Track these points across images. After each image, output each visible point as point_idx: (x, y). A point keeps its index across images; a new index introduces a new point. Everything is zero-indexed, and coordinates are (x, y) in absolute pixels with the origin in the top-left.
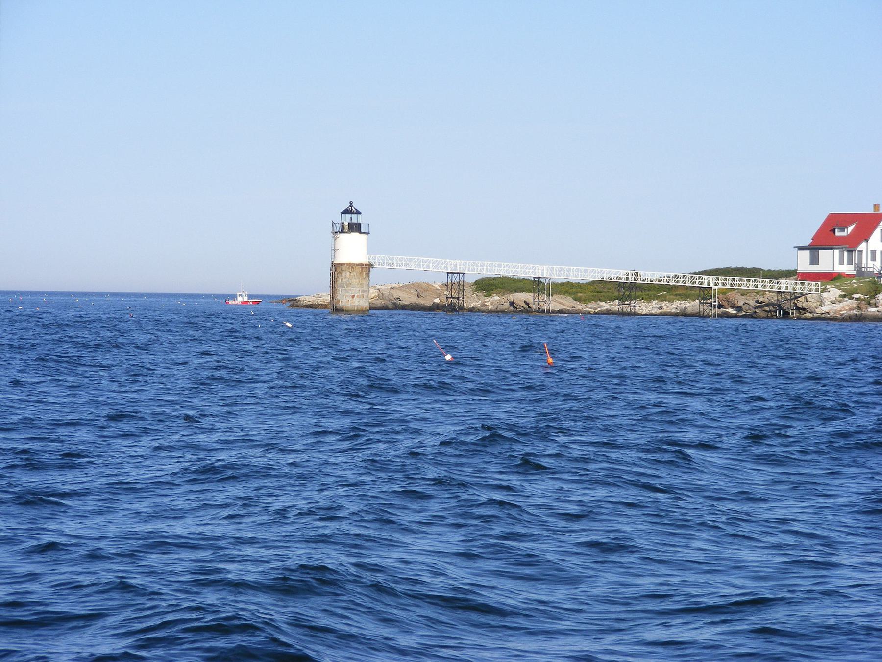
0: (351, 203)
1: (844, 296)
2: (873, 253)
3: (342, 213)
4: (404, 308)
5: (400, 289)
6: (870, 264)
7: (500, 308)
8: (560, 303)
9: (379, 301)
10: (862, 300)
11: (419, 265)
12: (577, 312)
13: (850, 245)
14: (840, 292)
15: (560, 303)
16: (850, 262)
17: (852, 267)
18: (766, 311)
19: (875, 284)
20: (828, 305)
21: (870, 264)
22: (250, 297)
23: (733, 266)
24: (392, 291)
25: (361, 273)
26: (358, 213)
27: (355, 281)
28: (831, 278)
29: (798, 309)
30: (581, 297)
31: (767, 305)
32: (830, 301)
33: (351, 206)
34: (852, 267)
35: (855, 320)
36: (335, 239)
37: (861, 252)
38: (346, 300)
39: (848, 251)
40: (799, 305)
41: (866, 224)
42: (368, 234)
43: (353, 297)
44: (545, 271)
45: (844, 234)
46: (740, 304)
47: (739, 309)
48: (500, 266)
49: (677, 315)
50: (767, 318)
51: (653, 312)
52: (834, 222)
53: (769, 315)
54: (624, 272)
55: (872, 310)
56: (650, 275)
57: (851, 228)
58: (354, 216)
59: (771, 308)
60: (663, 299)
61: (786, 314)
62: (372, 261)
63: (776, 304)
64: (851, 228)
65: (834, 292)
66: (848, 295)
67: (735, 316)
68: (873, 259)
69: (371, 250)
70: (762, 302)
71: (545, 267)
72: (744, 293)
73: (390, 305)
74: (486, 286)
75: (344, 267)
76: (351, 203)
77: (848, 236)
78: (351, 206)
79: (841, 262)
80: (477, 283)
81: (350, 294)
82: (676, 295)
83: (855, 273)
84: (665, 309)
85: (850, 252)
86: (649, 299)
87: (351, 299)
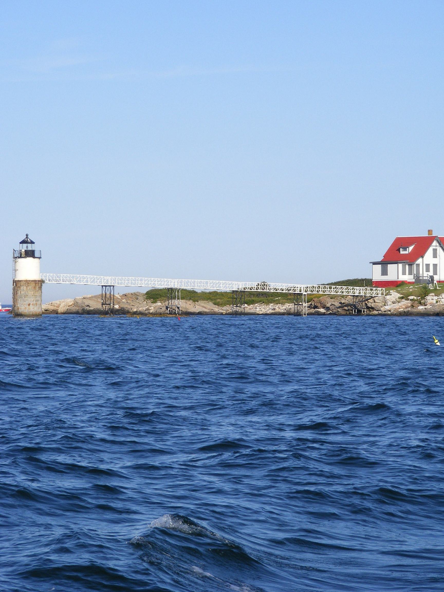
0: (27, 235)
1: (402, 298)
2: (428, 266)
3: (20, 243)
4: (89, 312)
5: (90, 298)
6: (425, 274)
7: (159, 311)
8: (203, 307)
9: (75, 308)
10: (415, 300)
11: (80, 281)
12: (214, 314)
13: (409, 261)
14: (399, 295)
15: (203, 307)
16: (410, 273)
17: (412, 277)
18: (345, 310)
19: (424, 288)
20: (390, 305)
21: (425, 274)
22: (3, 306)
23: (360, 278)
24: (84, 300)
25: (35, 287)
26: (32, 242)
27: (31, 293)
28: (396, 285)
29: (368, 308)
30: (219, 302)
31: (346, 306)
32: (392, 302)
33: (27, 238)
34: (412, 277)
35: (404, 315)
36: (15, 262)
37: (418, 265)
38: (23, 308)
39: (409, 265)
40: (369, 305)
41: (422, 244)
42: (40, 258)
43: (29, 305)
44: (176, 283)
45: (406, 252)
46: (328, 305)
47: (328, 309)
48: (141, 280)
49: (283, 314)
50: (346, 315)
51: (268, 312)
52: (400, 243)
53: (348, 313)
54: (256, 284)
55: (421, 308)
56: (277, 285)
57: (411, 248)
58: (29, 245)
59: (349, 308)
60: (278, 302)
61: (359, 311)
62: (44, 278)
63: (352, 305)
64: (411, 248)
65: (395, 295)
66: (405, 297)
67: (324, 314)
68: (428, 270)
69: (42, 270)
70: (344, 303)
71: (176, 280)
72: (332, 297)
73: (80, 311)
74: (154, 295)
75: (22, 283)
76: (27, 235)
77: (409, 254)
78: (27, 238)
79: (404, 273)
80: (148, 293)
81: (27, 302)
82: (288, 299)
83: (414, 280)
84: (277, 310)
85: (410, 265)
86: (268, 303)
87: (27, 307)
